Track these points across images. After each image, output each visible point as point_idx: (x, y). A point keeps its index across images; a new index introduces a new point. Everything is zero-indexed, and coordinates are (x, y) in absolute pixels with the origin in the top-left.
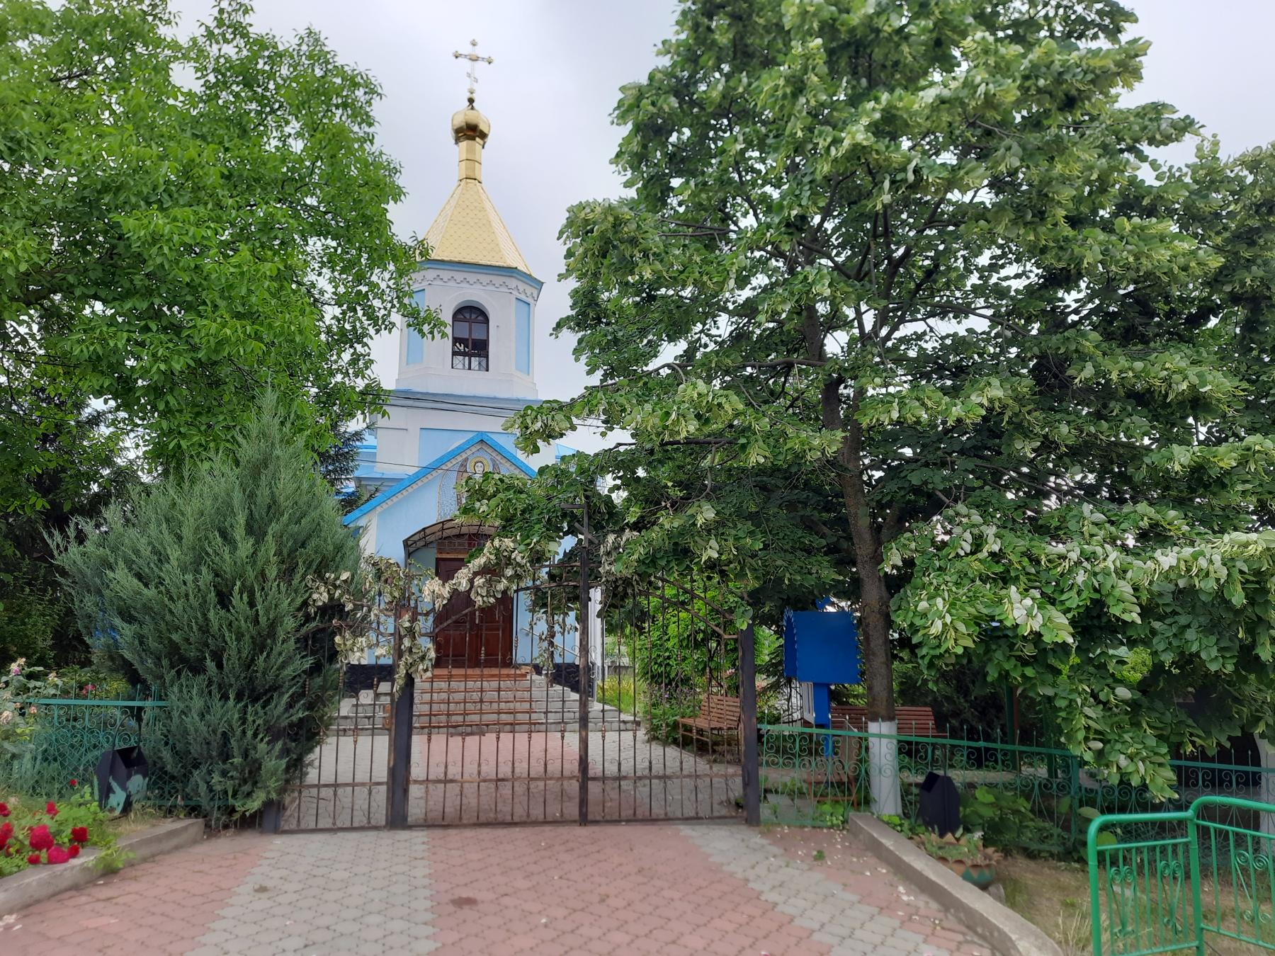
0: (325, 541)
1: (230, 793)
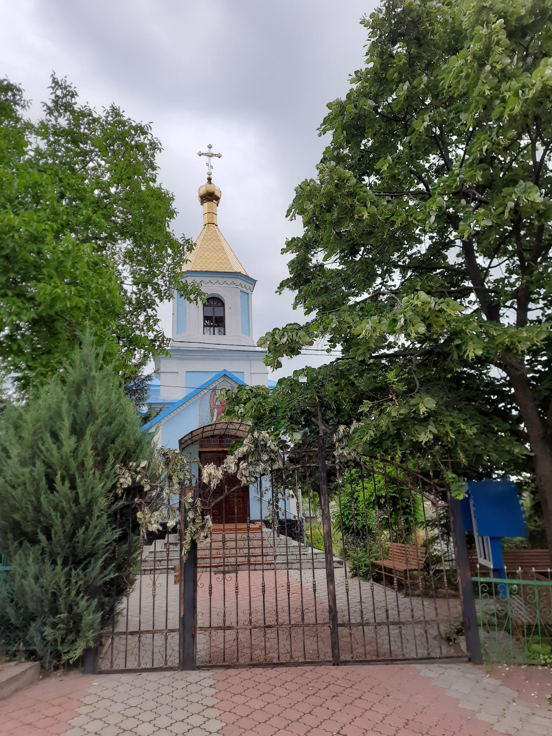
0: (129, 437)
1: (59, 641)
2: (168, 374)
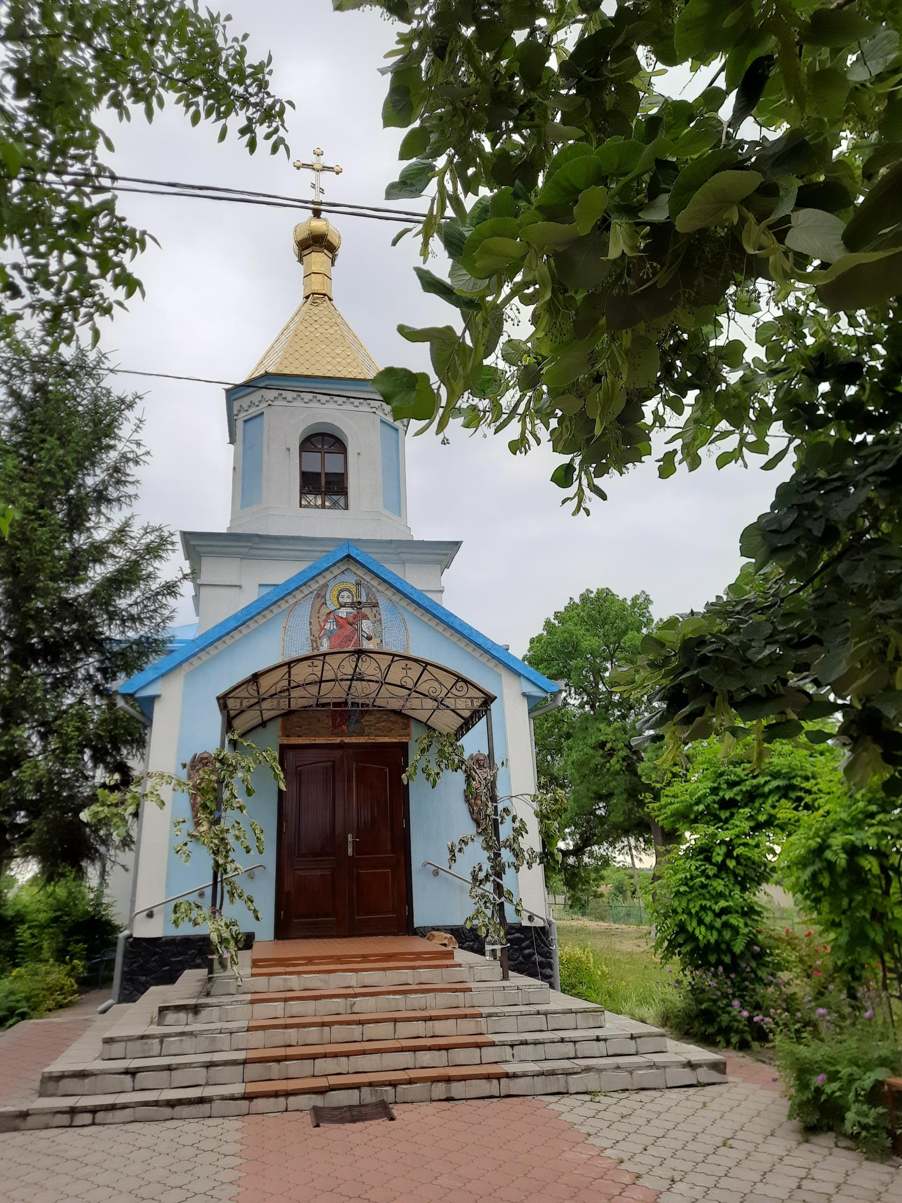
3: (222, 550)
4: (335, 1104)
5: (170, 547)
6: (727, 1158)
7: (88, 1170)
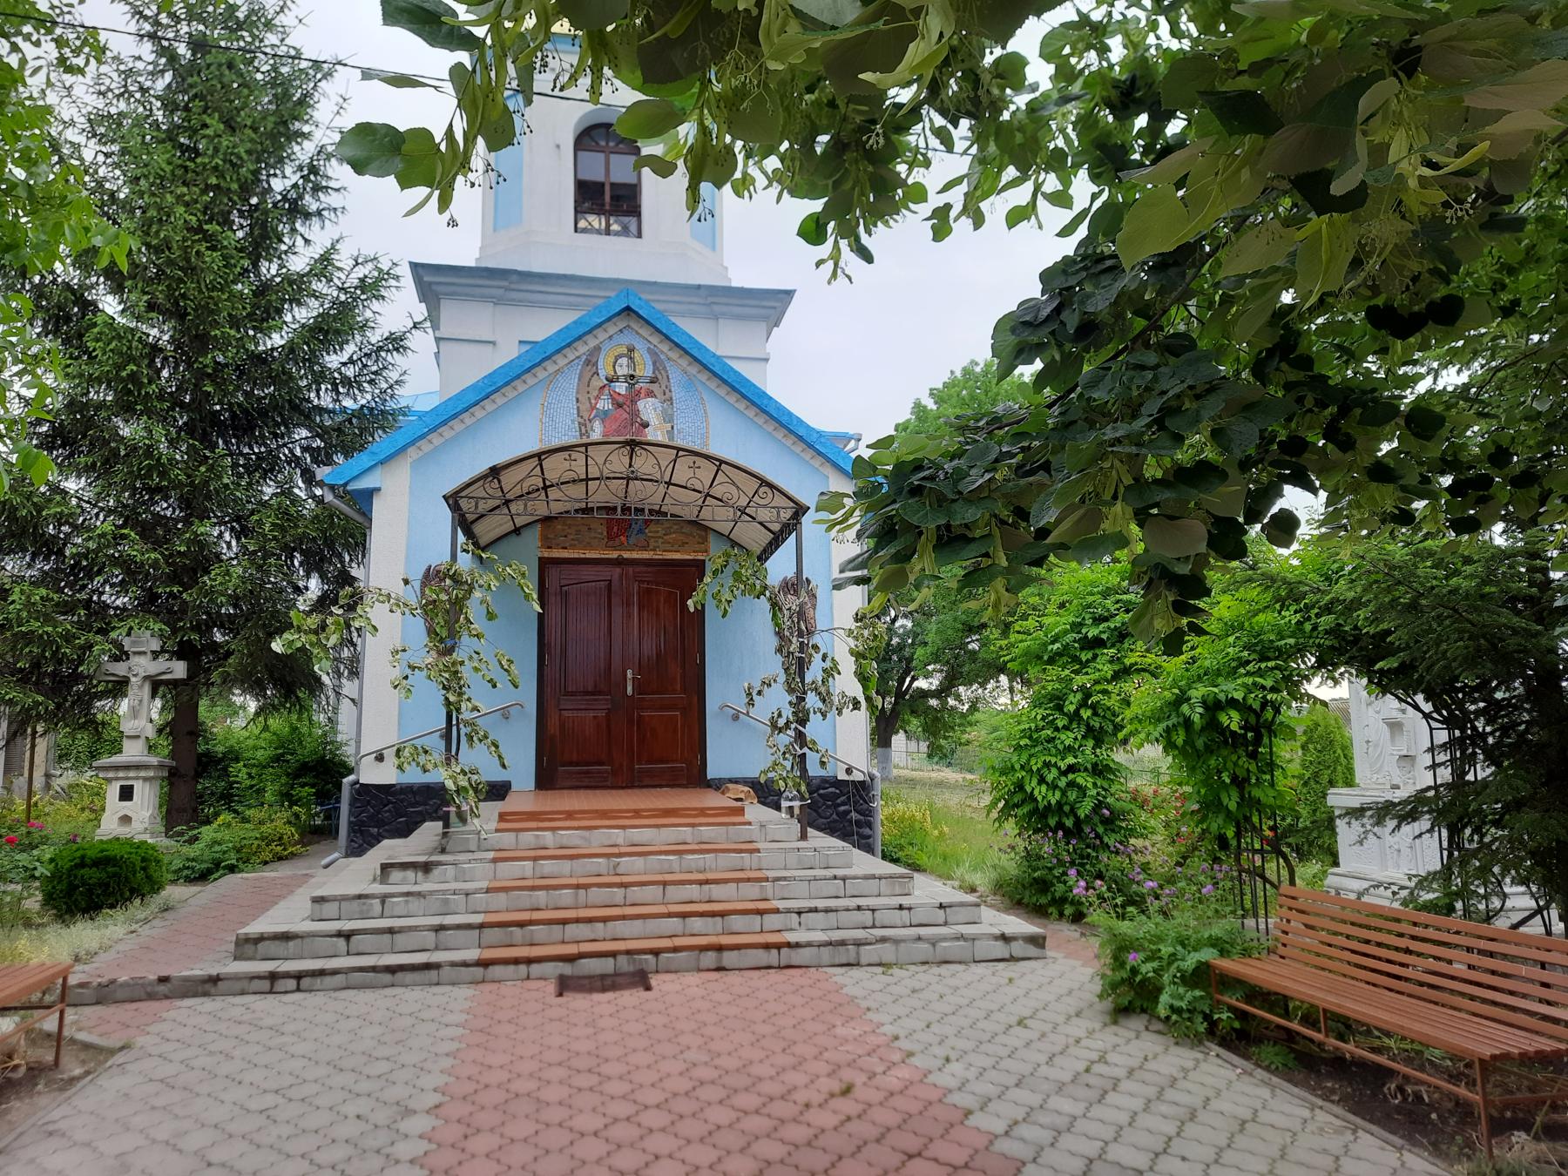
2: (466, 345)
3: (467, 290)
4: (586, 972)
5: (392, 282)
6: (1018, 1036)
7: (284, 1039)
